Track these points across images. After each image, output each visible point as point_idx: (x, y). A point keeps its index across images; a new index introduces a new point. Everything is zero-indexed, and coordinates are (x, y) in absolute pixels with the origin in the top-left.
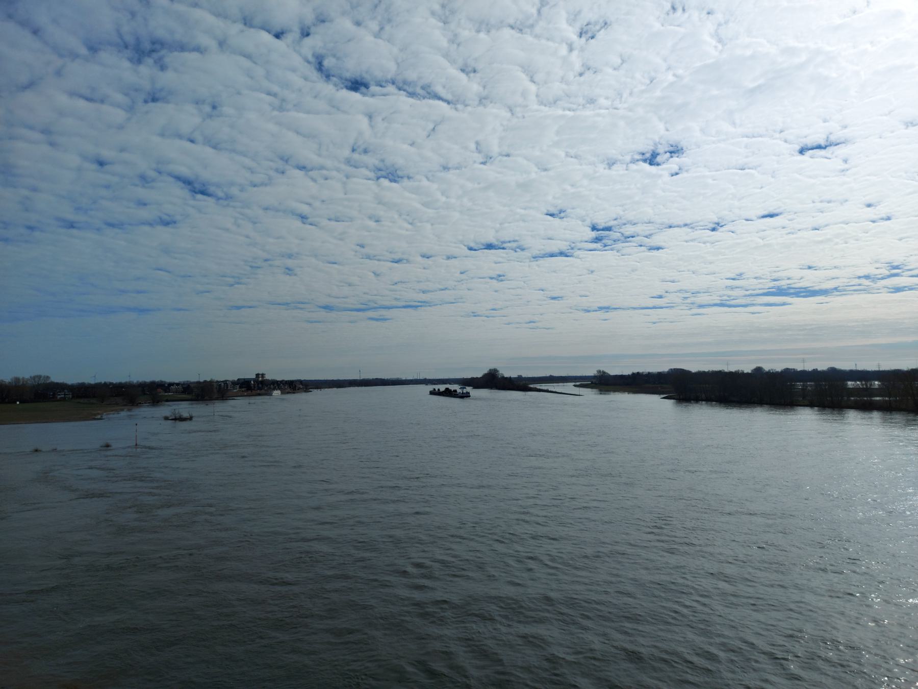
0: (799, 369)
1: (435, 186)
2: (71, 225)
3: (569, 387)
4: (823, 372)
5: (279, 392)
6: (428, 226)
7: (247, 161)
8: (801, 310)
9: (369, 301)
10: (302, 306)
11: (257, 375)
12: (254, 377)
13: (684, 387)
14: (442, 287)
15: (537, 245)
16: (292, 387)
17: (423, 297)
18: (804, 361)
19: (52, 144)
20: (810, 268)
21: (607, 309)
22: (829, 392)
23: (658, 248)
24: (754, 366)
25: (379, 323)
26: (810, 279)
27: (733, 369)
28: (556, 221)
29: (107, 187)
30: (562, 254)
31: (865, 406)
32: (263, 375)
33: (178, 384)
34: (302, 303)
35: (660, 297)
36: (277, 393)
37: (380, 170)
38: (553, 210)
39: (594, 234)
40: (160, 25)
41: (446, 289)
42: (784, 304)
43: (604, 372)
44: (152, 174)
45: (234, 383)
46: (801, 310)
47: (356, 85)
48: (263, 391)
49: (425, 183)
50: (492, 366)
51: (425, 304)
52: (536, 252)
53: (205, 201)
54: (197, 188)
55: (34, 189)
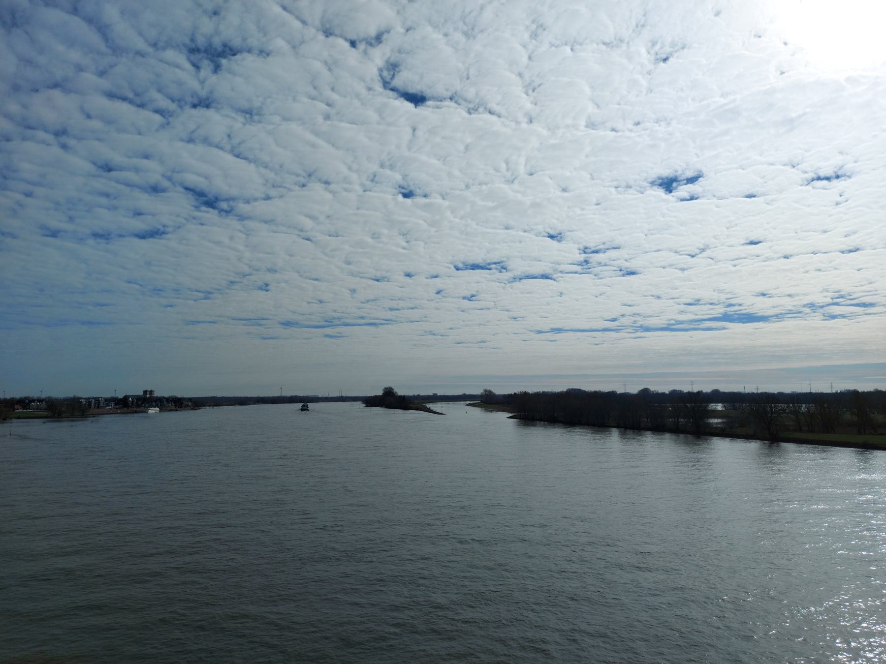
0: (685, 391)
1: (446, 203)
2: (54, 234)
3: (460, 408)
4: (864, 394)
5: (157, 410)
6: (422, 244)
7: (271, 175)
8: (738, 335)
9: (334, 318)
10: (263, 322)
11: (145, 392)
12: (141, 393)
13: (537, 409)
14: (411, 306)
15: (519, 267)
16: (177, 403)
17: (389, 315)
18: (692, 383)
19: (64, 147)
20: (764, 295)
21: (559, 330)
22: (682, 416)
23: (633, 273)
24: (641, 388)
25: (333, 340)
26: (761, 306)
27: (695, 390)
28: (554, 243)
29: (107, 195)
30: (545, 277)
31: (659, 429)
32: (151, 392)
33: (40, 400)
34: (264, 319)
35: (614, 320)
36: (153, 411)
37: (403, 188)
38: (552, 232)
39: (582, 257)
40: (229, 29)
41: (416, 308)
42: (724, 328)
43: (490, 392)
44: (166, 183)
45: (108, 401)
46: (738, 335)
47: (417, 99)
48: (142, 409)
49: (439, 201)
50: (388, 385)
51: (388, 321)
52: (518, 273)
53: (207, 212)
54: (208, 200)
55: (28, 195)
